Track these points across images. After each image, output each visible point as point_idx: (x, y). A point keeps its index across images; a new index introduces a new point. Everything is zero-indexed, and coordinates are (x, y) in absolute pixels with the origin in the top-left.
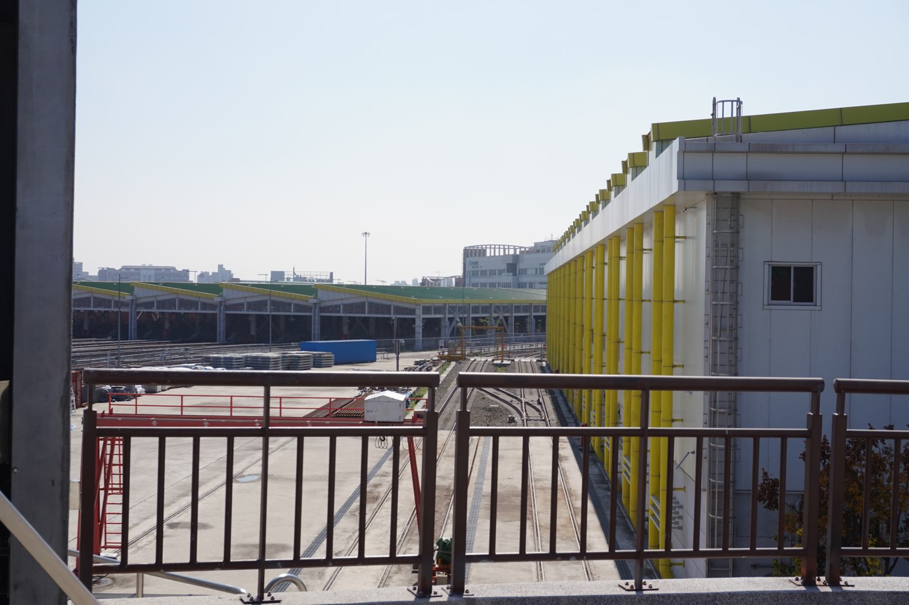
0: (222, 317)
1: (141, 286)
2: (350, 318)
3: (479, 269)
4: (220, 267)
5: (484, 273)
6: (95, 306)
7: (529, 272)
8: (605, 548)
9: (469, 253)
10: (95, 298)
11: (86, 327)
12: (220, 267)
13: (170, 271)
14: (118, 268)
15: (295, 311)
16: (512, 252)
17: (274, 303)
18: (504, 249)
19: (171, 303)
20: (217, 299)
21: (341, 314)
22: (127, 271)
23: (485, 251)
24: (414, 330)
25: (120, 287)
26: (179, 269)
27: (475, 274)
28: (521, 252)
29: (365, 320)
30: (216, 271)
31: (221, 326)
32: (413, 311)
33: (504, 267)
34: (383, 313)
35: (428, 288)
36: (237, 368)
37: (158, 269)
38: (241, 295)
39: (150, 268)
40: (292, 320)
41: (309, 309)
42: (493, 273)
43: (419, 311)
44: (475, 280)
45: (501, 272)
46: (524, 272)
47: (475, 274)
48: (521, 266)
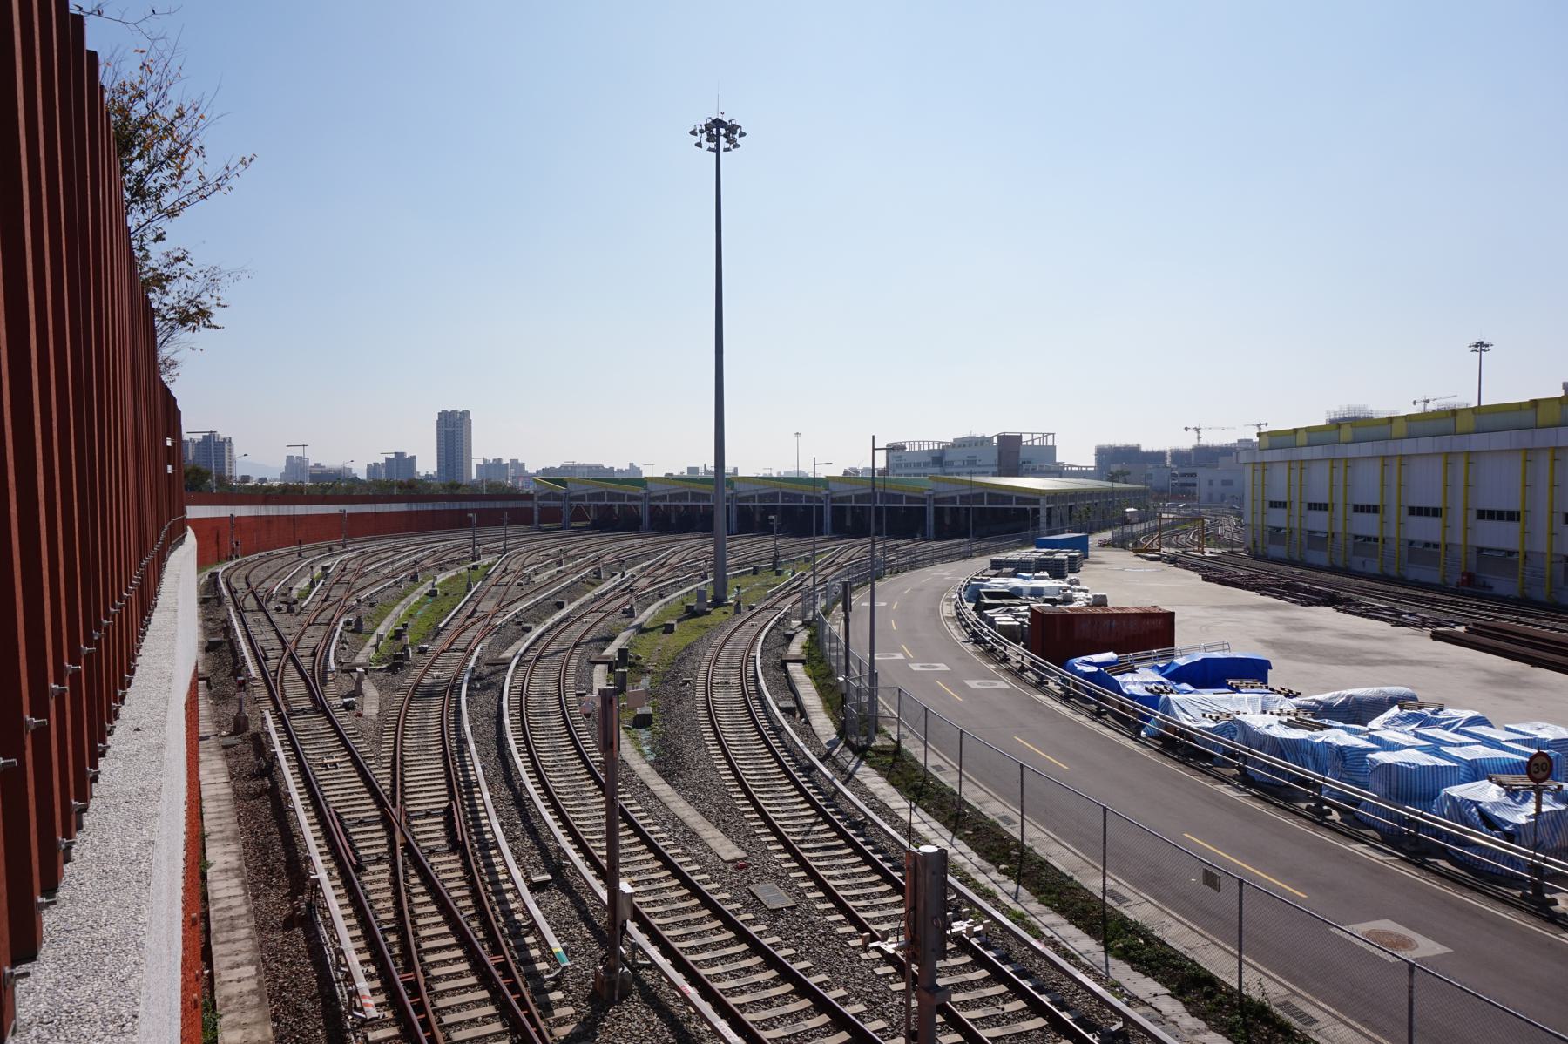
1: (573, 481)
2: (889, 509)
5: (908, 465)
8: (790, 666)
11: (673, 521)
13: (599, 468)
14: (1321, 421)
17: (784, 495)
19: (683, 496)
20: (642, 492)
22: (564, 469)
25: (561, 482)
27: (899, 466)
31: (930, 519)
32: (1037, 502)
33: (929, 459)
35: (850, 477)
36: (269, 520)
37: (590, 467)
38: (848, 487)
39: (583, 467)
41: (924, 501)
42: (917, 465)
43: (1042, 501)
44: (899, 471)
45: (926, 465)
46: (951, 464)
47: (899, 466)
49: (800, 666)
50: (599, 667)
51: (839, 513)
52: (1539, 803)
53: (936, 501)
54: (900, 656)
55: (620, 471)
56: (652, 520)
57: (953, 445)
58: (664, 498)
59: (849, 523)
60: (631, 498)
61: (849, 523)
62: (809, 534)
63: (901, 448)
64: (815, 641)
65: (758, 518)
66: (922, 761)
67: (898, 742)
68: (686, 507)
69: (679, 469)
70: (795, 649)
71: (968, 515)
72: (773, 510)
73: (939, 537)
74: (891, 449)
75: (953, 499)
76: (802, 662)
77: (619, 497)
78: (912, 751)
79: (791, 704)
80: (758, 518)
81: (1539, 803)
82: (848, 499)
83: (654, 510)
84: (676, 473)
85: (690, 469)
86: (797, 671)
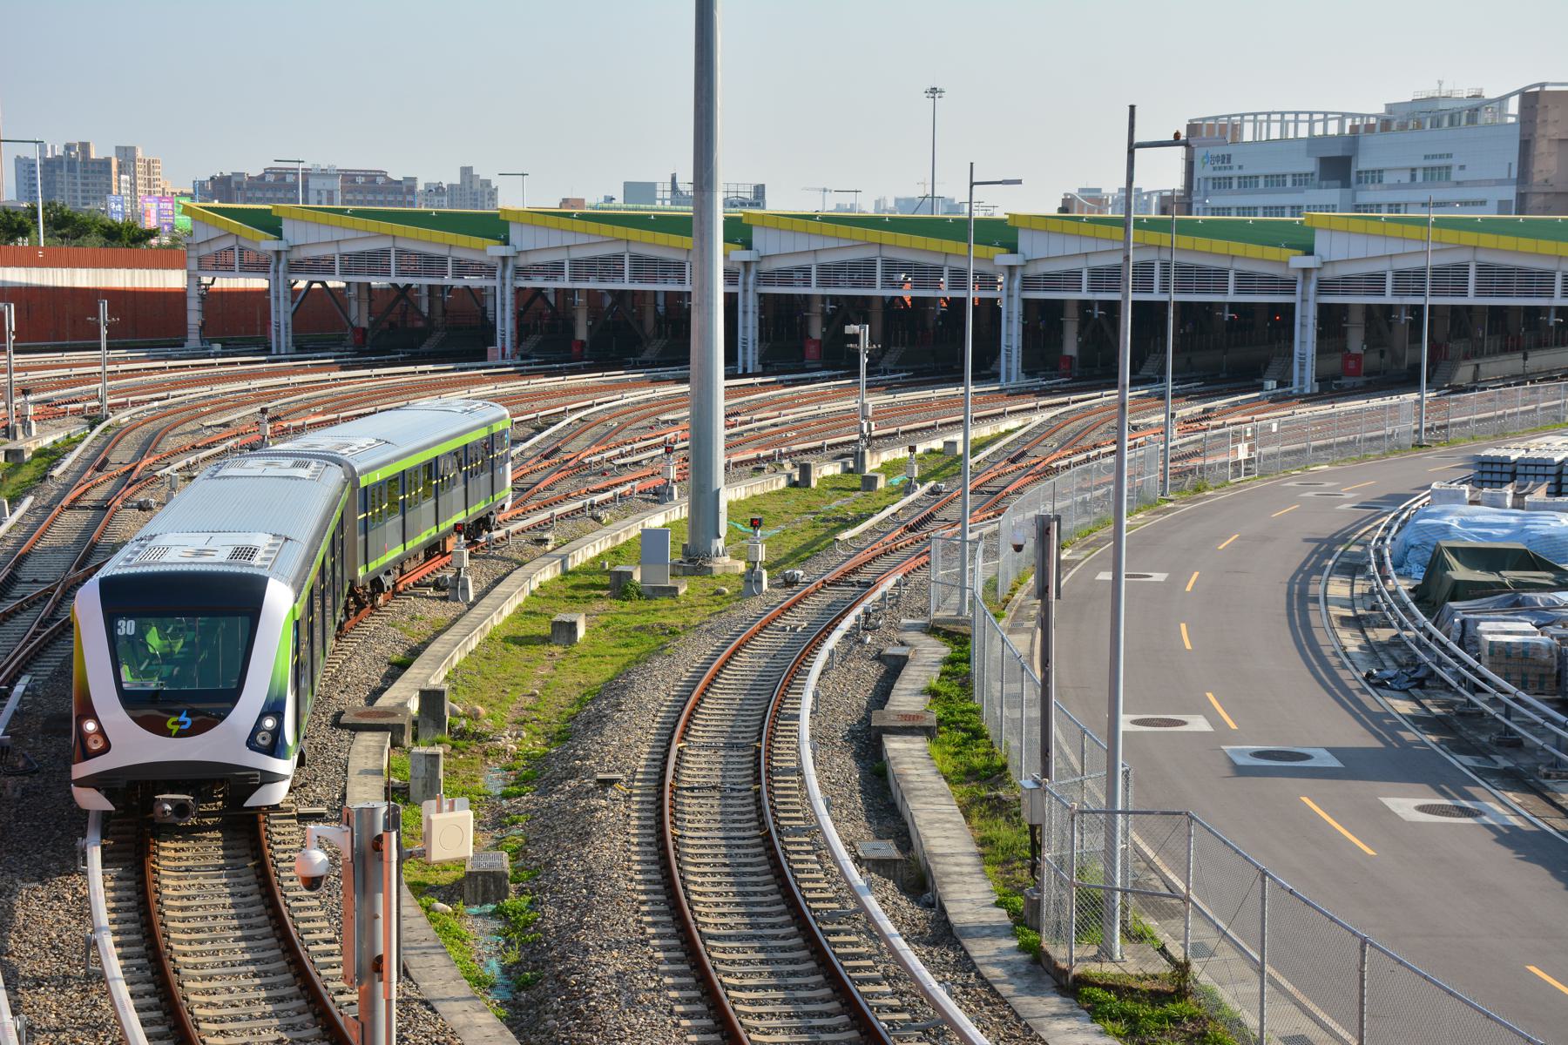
0: (1312, 312)
3: (1235, 172)
4: (466, 172)
5: (1248, 182)
6: (573, 279)
7: (1388, 178)
8: (894, 746)
9: (127, 155)
10: (401, 253)
11: (582, 334)
12: (466, 172)
15: (1239, 291)
16: (1333, 129)
17: (638, 261)
18: (1311, 123)
21: (1388, 299)
23: (1237, 129)
24: (204, 312)
26: (396, 176)
28: (1354, 128)
29: (1389, 309)
30: (457, 181)
33: (1310, 166)
34: (1529, 295)
40: (1097, 312)
41: (1288, 286)
42: (1275, 181)
45: (1301, 180)
47: (1222, 184)
48: (1363, 163)
49: (918, 744)
50: (367, 739)
51: (1043, 320)
52: (994, 932)
53: (1324, 287)
54: (1198, 724)
55: (436, 190)
56: (523, 331)
57: (1386, 124)
58: (555, 269)
59: (1071, 347)
60: (462, 268)
61: (1071, 347)
62: (979, 222)
63: (1226, 130)
64: (959, 671)
65: (816, 331)
66: (1252, 1022)
67: (1182, 968)
68: (619, 295)
69: (600, 188)
70: (907, 699)
71: (1416, 326)
72: (858, 309)
73: (1329, 388)
74: (1192, 139)
75: (1375, 283)
76: (928, 732)
77: (432, 264)
78: (1225, 995)
79: (888, 849)
80: (816, 331)
81: (994, 932)
82: (1070, 279)
83: (528, 301)
84: (593, 199)
85: (632, 190)
86: (907, 756)
